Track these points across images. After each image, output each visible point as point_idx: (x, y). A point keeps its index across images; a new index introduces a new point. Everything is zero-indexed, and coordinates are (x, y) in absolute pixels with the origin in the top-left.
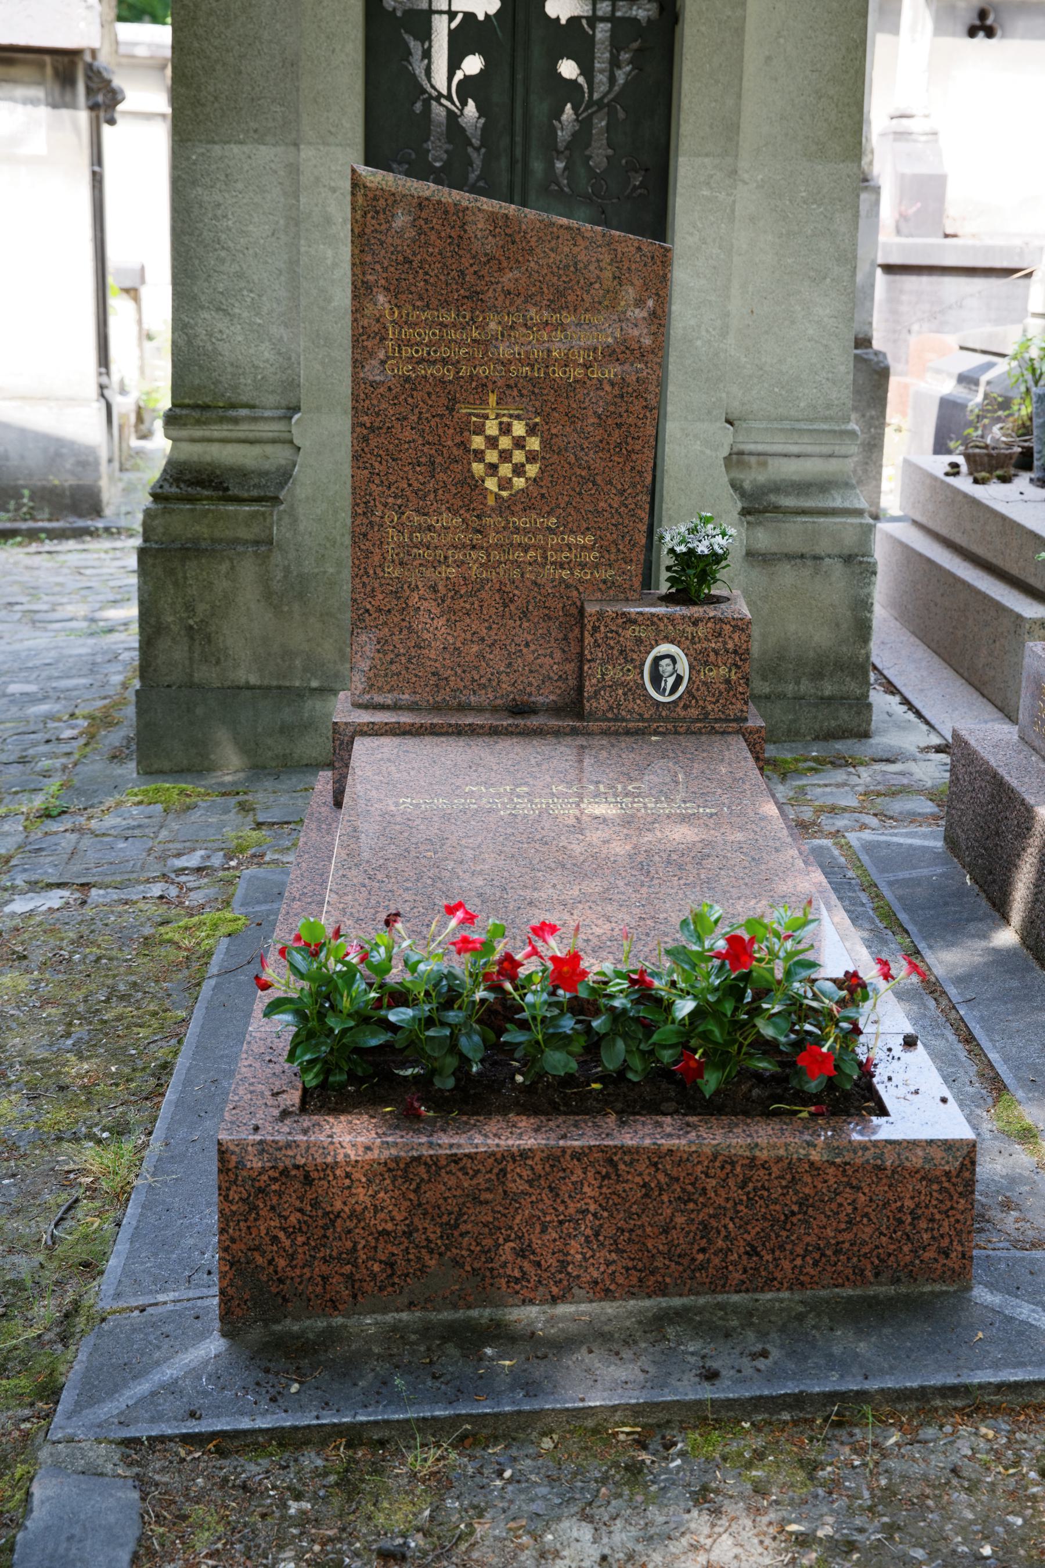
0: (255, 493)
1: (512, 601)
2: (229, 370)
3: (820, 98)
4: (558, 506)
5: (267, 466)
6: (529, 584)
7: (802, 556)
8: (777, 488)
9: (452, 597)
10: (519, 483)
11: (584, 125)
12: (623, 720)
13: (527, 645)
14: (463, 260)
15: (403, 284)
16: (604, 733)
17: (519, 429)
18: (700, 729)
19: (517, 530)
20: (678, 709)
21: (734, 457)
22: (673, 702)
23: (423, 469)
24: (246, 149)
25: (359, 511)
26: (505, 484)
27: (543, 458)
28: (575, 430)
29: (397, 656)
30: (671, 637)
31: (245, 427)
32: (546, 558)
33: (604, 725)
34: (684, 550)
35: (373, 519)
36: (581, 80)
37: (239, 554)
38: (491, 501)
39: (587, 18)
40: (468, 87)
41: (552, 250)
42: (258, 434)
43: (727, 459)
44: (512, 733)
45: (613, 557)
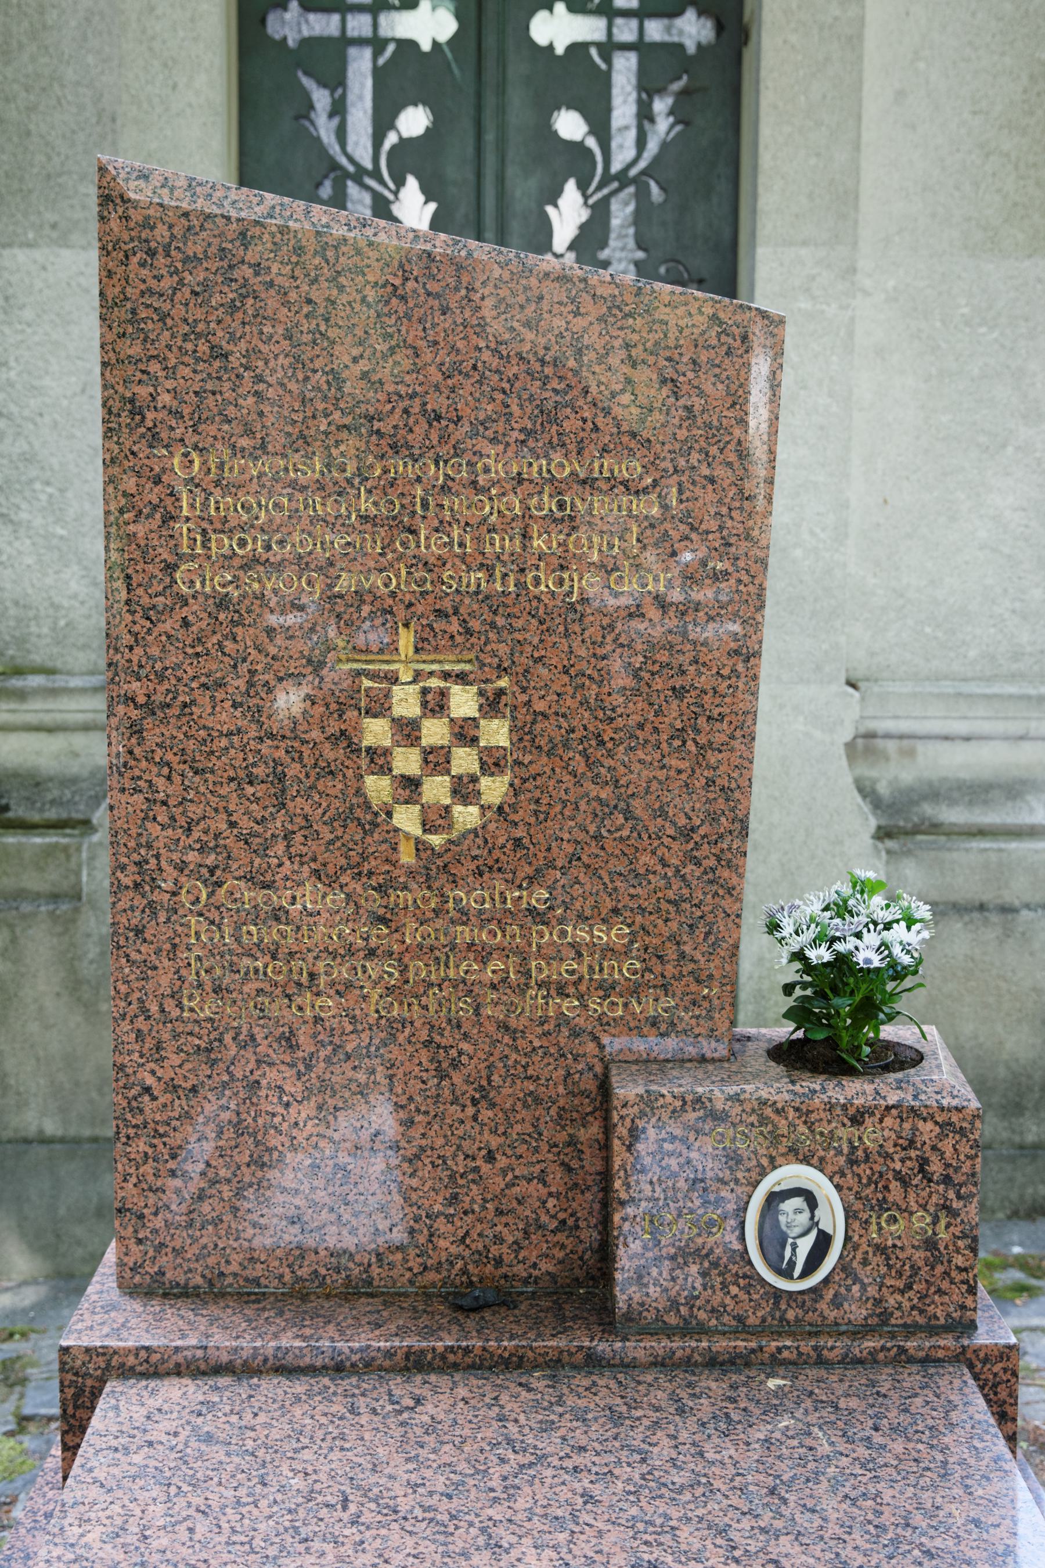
0: (52, 814)
1: (455, 1064)
2: (13, 611)
3: (988, 155)
4: (551, 865)
5: (74, 768)
6: (491, 1028)
7: (982, 907)
8: (934, 793)
9: (328, 1060)
10: (467, 816)
11: (600, 213)
12: (702, 1330)
13: (490, 1158)
14: (338, 349)
15: (210, 401)
16: (661, 1363)
17: (464, 702)
18: (873, 1353)
19: (464, 916)
20: (822, 1306)
21: (860, 741)
22: (813, 1290)
23: (260, 790)
24: (37, 254)
25: (127, 881)
26: (436, 819)
27: (518, 763)
28: (584, 703)
29: (213, 1183)
30: (803, 1150)
31: (37, 704)
32: (528, 974)
33: (661, 1346)
34: (827, 957)
35: (156, 896)
36: (591, 143)
37: (24, 917)
38: (407, 856)
39: (598, 45)
40: (408, 159)
41: (527, 324)
42: (59, 717)
43: (850, 747)
44: (455, 1366)
45: (670, 970)
